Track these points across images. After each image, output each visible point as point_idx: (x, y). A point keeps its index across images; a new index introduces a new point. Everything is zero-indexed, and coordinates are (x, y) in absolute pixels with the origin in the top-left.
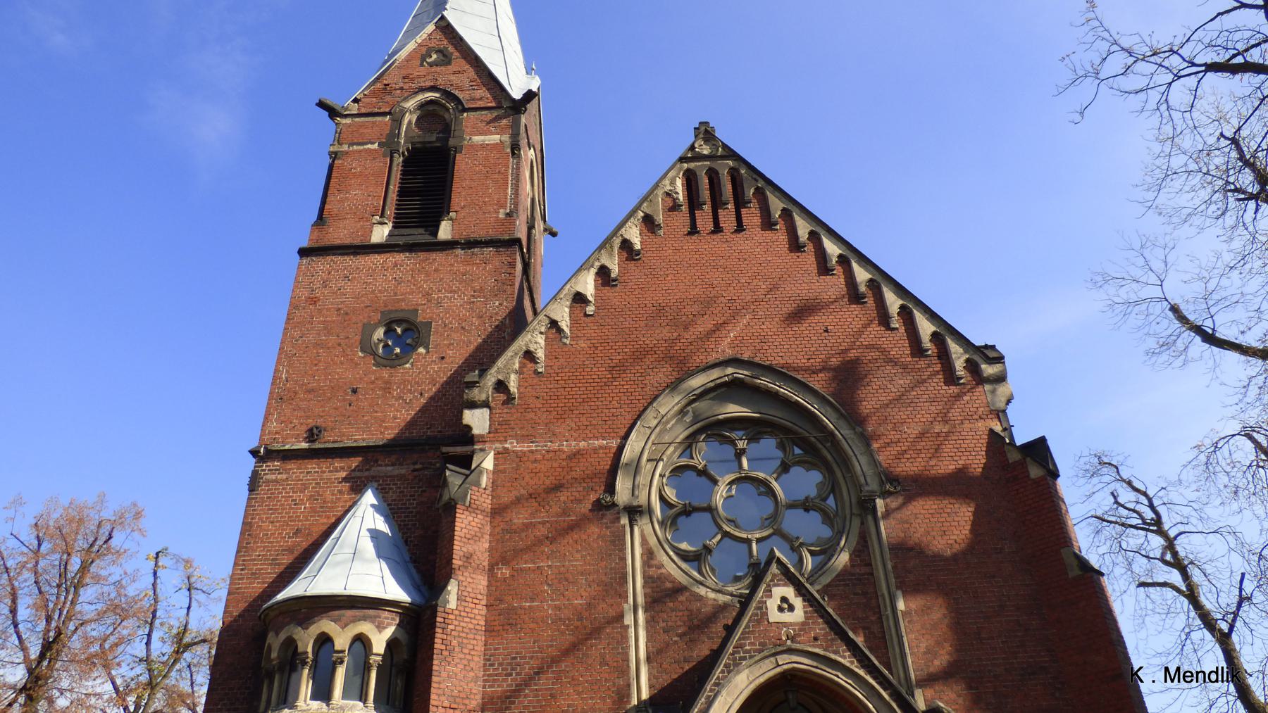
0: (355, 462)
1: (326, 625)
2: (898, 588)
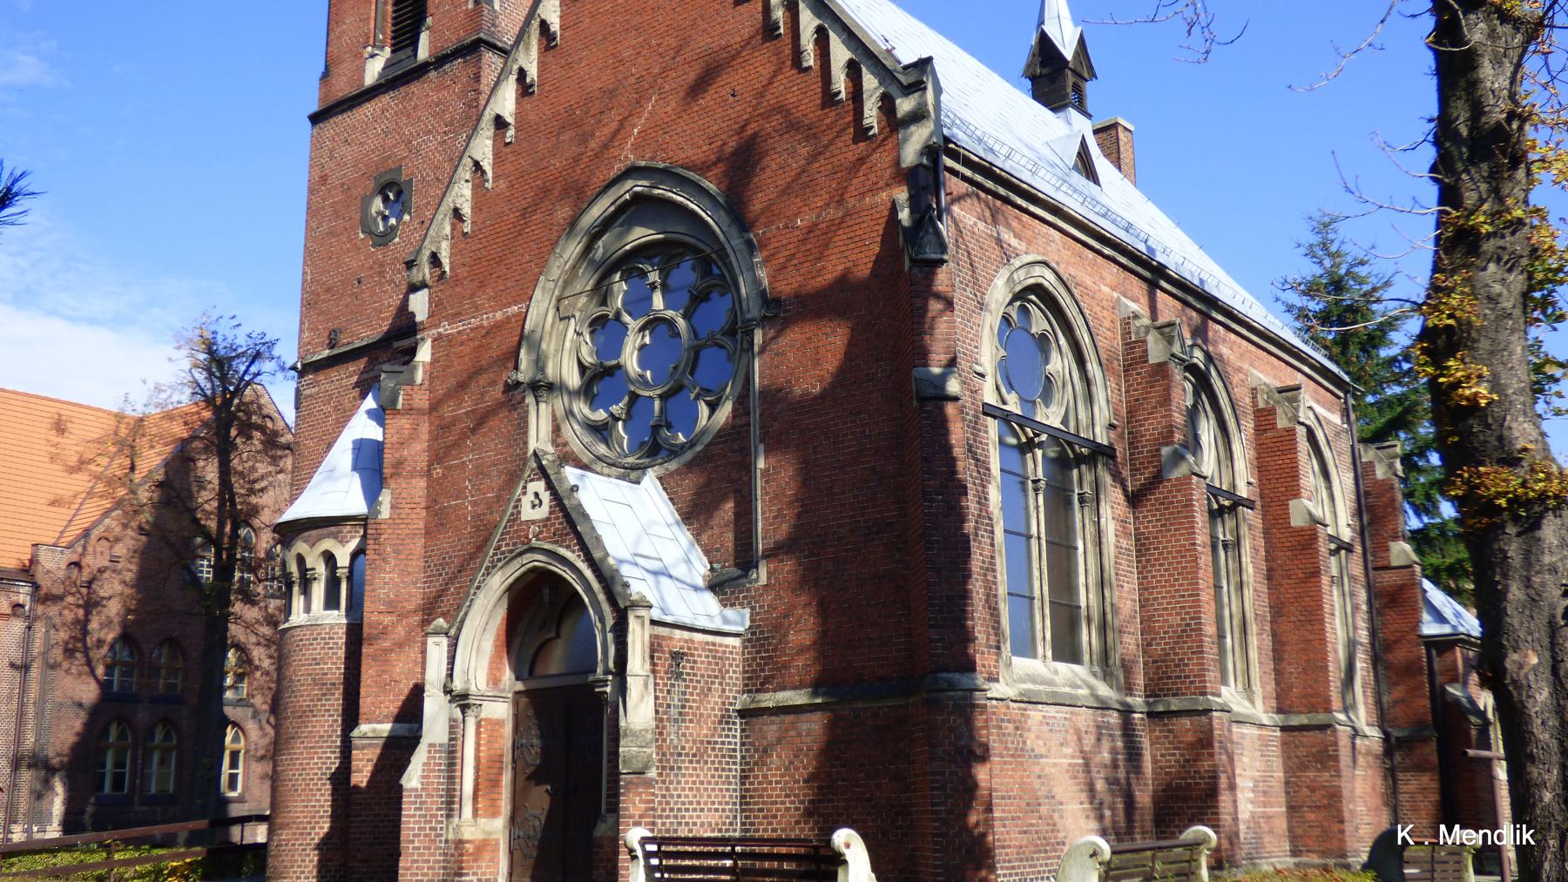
0: (361, 364)
2: (762, 441)
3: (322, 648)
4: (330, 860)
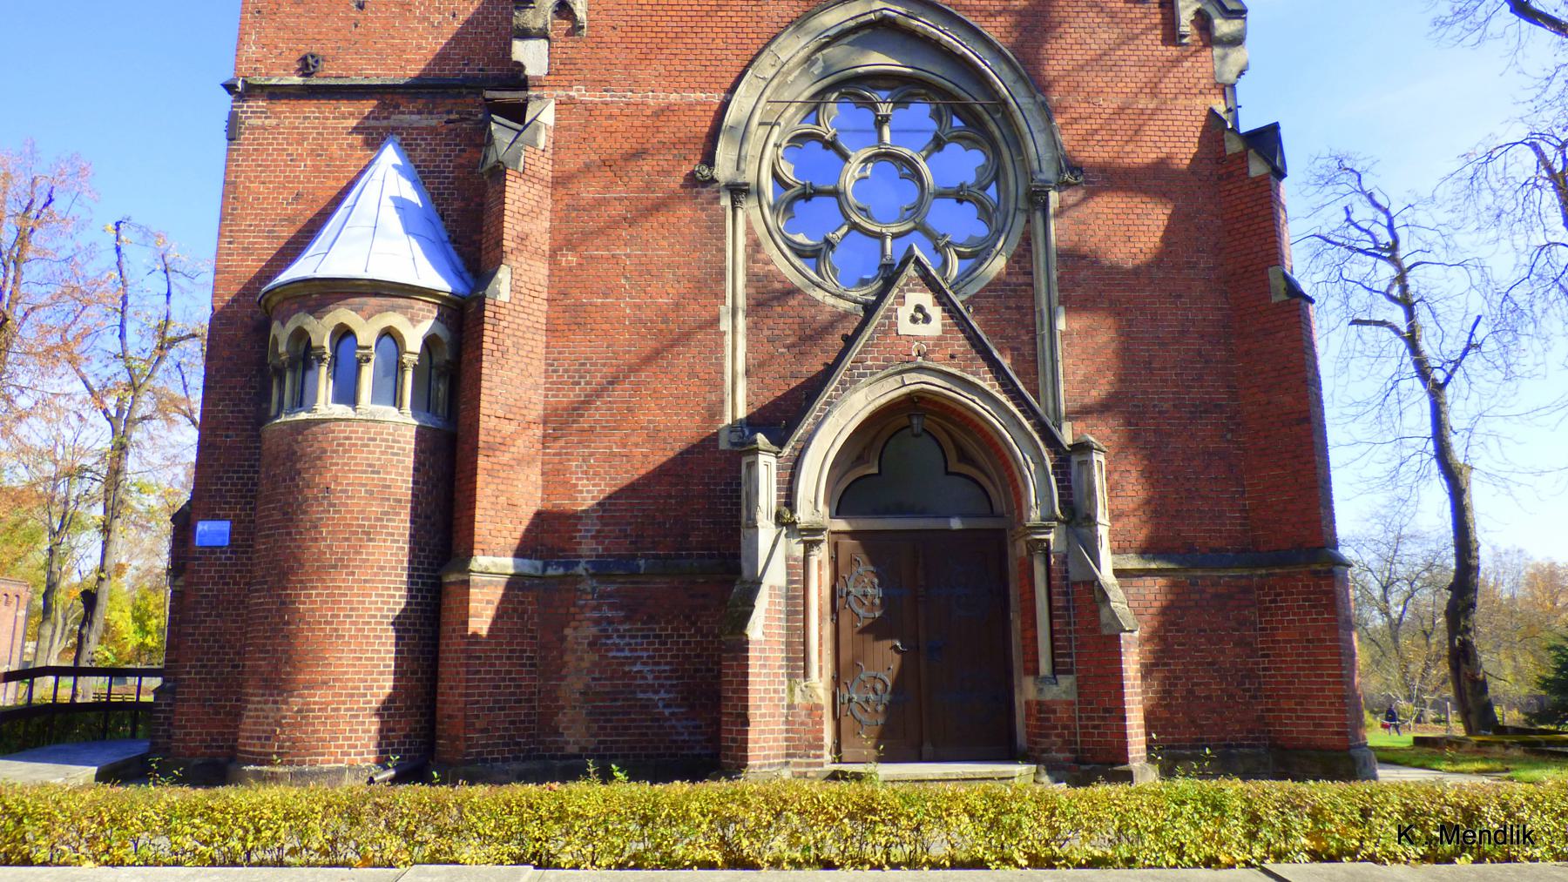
0: (368, 106)
1: (343, 314)
2: (1060, 303)
3: (382, 453)
4: (393, 730)
